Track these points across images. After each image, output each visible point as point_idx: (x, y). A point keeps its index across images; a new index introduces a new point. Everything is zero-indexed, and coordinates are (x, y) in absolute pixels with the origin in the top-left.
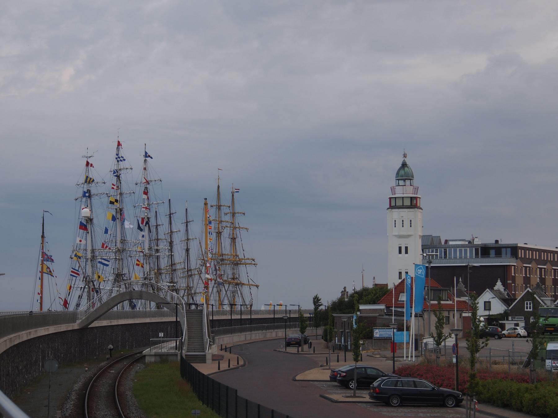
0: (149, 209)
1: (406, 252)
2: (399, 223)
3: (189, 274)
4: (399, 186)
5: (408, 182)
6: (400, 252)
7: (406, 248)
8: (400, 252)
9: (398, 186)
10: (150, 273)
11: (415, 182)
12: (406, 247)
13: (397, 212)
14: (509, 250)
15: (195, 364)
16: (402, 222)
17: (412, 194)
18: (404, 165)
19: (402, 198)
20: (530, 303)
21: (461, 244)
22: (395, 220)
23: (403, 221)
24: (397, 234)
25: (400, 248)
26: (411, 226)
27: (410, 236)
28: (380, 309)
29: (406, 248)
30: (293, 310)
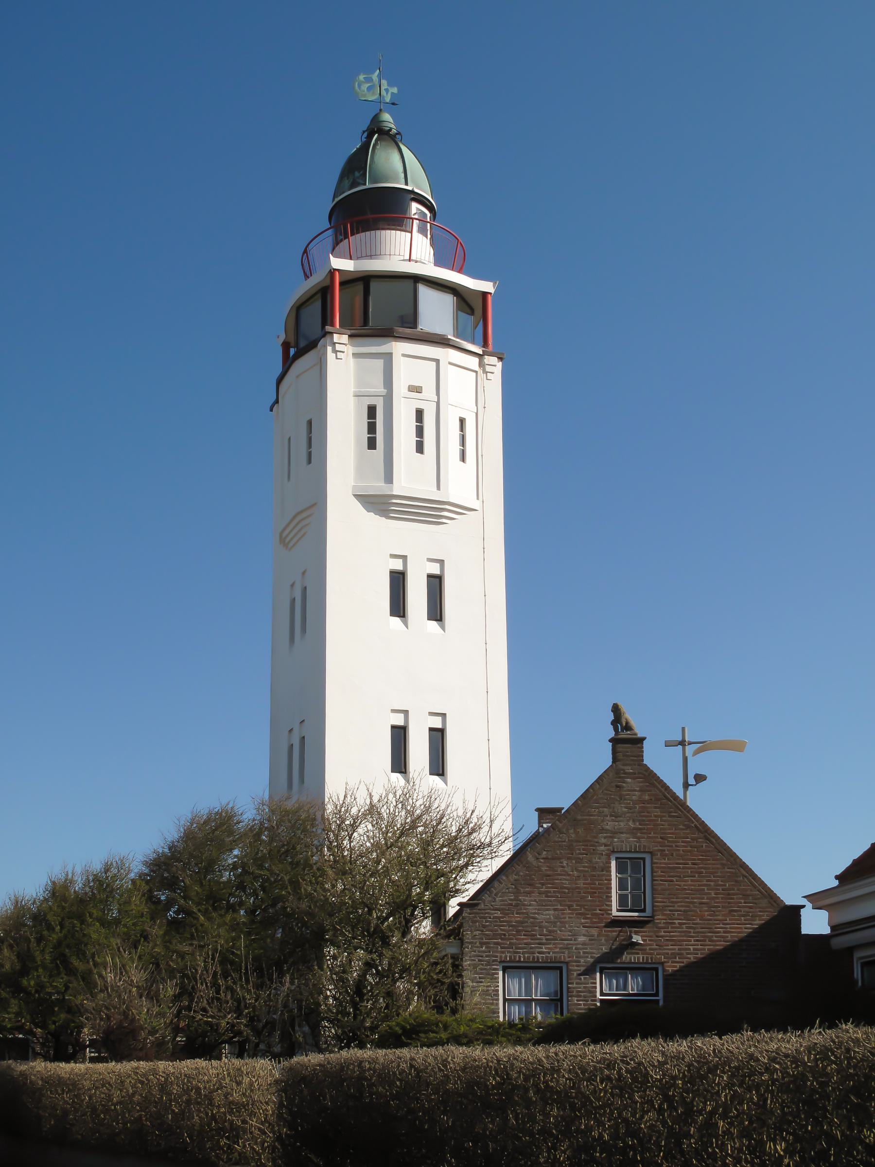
1: (436, 612)
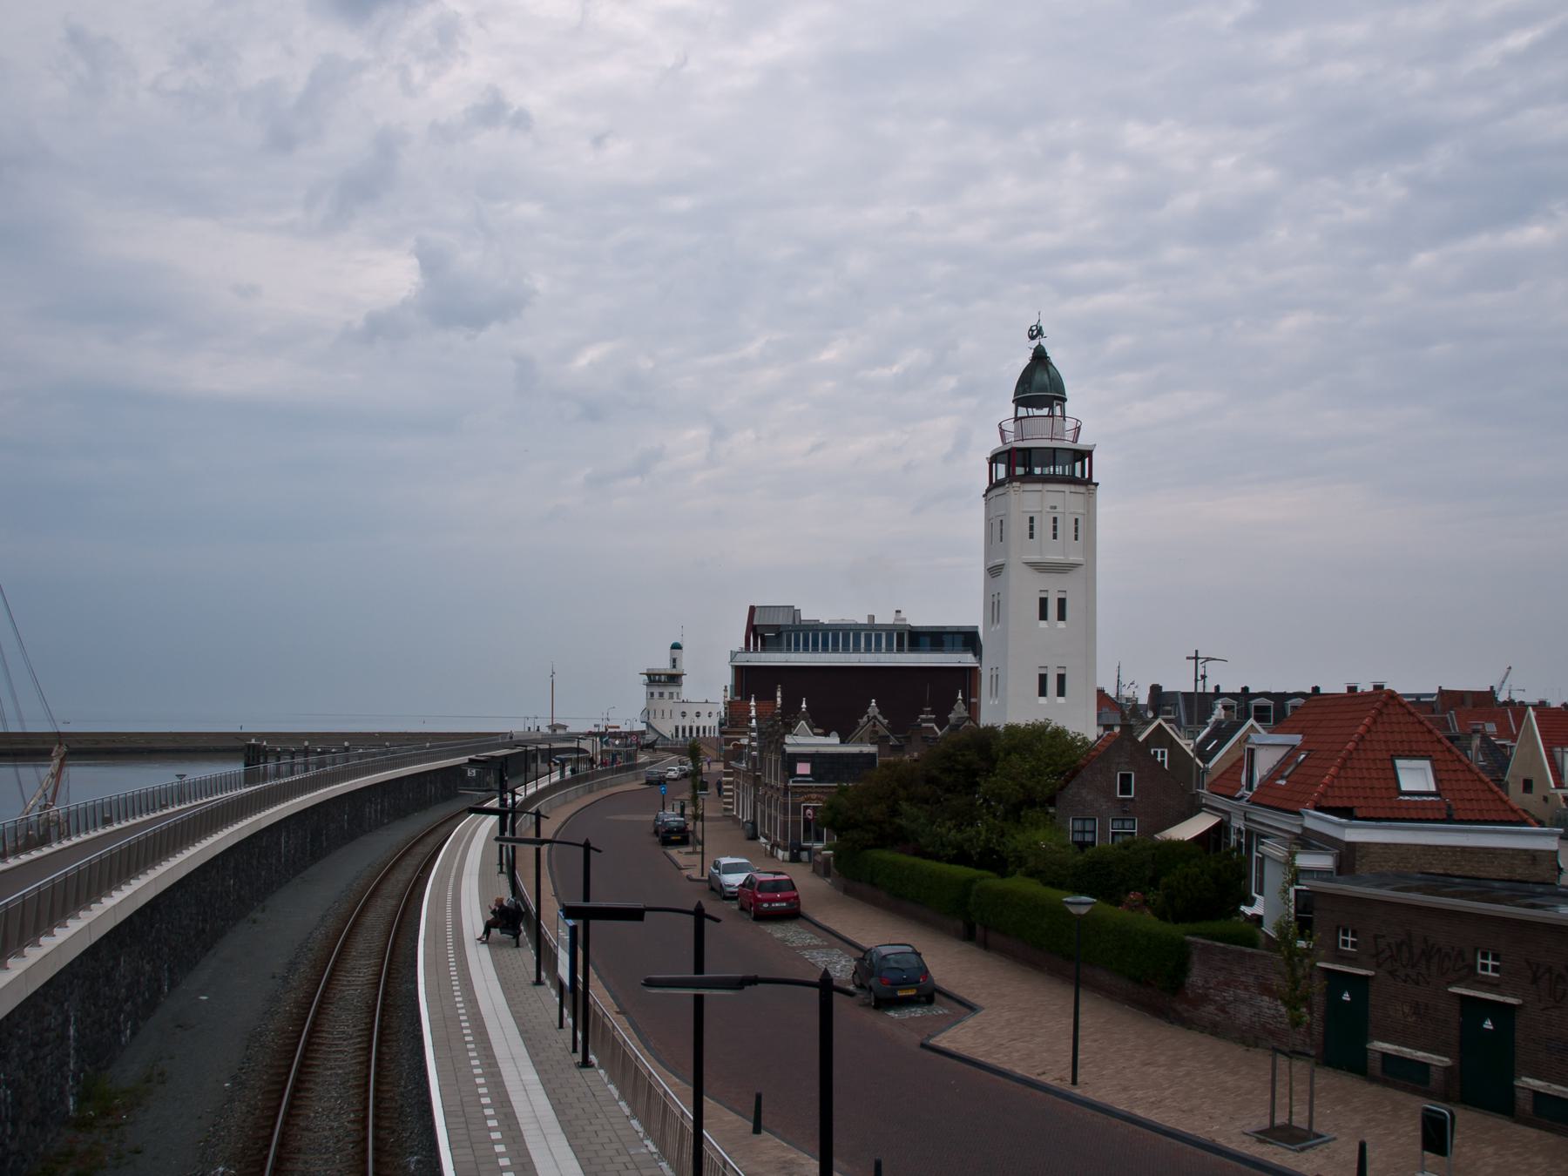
0: (1000, 424)
2: (1044, 527)
6: (1043, 615)
7: (1062, 603)
8: (1043, 615)
13: (1040, 491)
14: (961, 637)
16: (1058, 532)
18: (1040, 357)
19: (1052, 450)
20: (1163, 754)
22: (1032, 515)
23: (1055, 520)
24: (1036, 558)
25: (1043, 603)
27: (1074, 566)
28: (1526, 851)
29: (1062, 603)
30: (1041, 881)
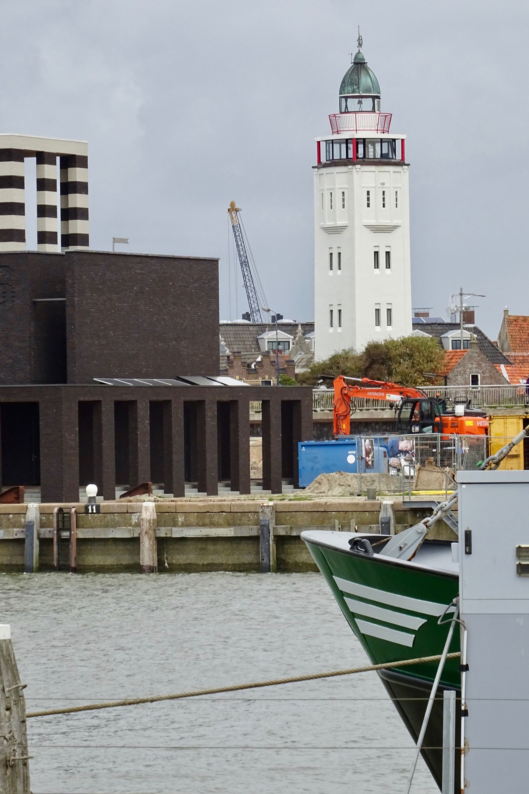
2: (376, 199)
3: (112, 307)
4: (348, 112)
5: (367, 104)
9: (345, 112)
10: (134, 306)
11: (385, 105)
12: (375, 252)
15: (349, 599)
17: (377, 130)
21: (78, 247)
24: (373, 222)
26: (368, 205)
27: (395, 227)
